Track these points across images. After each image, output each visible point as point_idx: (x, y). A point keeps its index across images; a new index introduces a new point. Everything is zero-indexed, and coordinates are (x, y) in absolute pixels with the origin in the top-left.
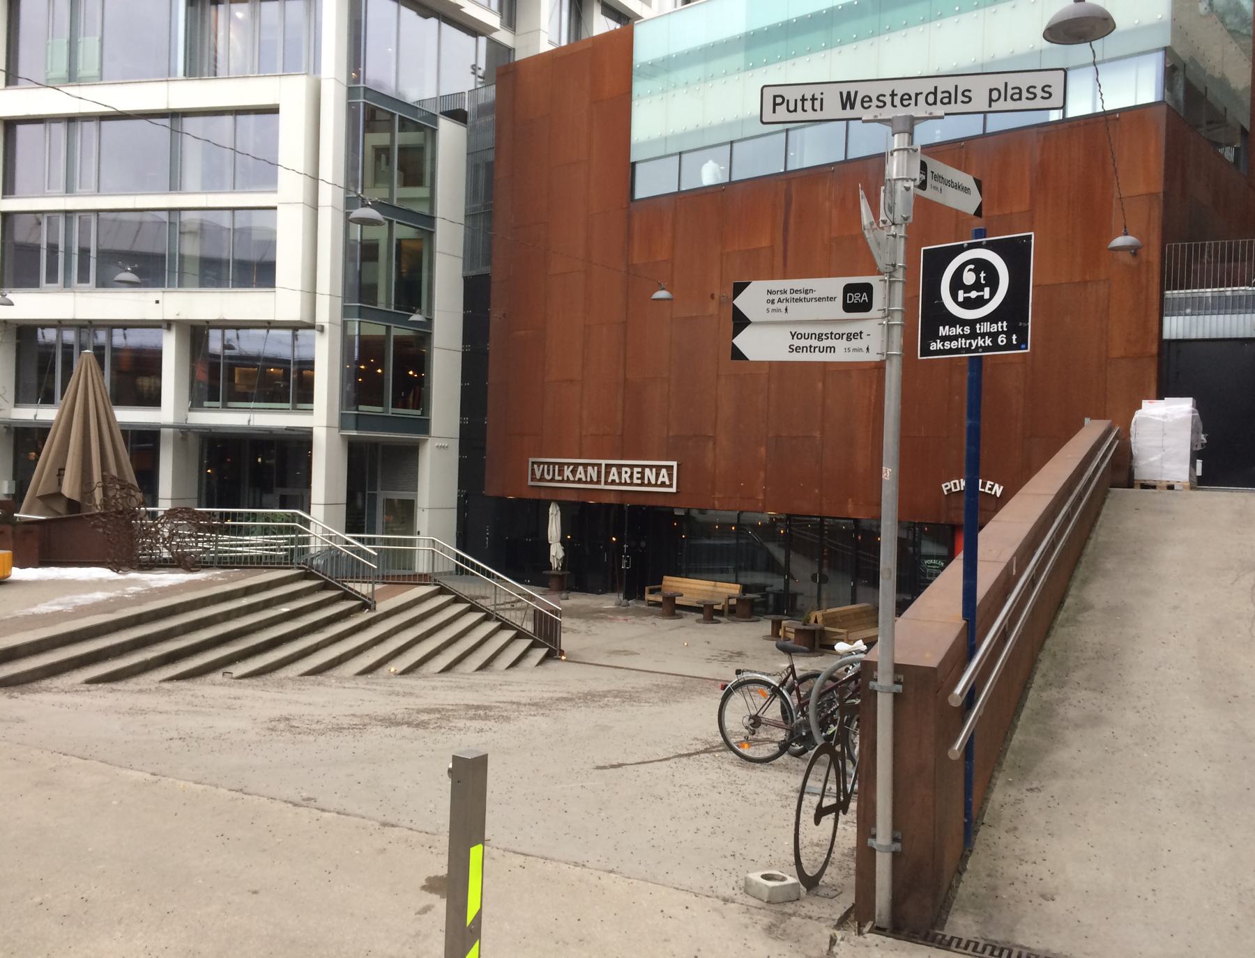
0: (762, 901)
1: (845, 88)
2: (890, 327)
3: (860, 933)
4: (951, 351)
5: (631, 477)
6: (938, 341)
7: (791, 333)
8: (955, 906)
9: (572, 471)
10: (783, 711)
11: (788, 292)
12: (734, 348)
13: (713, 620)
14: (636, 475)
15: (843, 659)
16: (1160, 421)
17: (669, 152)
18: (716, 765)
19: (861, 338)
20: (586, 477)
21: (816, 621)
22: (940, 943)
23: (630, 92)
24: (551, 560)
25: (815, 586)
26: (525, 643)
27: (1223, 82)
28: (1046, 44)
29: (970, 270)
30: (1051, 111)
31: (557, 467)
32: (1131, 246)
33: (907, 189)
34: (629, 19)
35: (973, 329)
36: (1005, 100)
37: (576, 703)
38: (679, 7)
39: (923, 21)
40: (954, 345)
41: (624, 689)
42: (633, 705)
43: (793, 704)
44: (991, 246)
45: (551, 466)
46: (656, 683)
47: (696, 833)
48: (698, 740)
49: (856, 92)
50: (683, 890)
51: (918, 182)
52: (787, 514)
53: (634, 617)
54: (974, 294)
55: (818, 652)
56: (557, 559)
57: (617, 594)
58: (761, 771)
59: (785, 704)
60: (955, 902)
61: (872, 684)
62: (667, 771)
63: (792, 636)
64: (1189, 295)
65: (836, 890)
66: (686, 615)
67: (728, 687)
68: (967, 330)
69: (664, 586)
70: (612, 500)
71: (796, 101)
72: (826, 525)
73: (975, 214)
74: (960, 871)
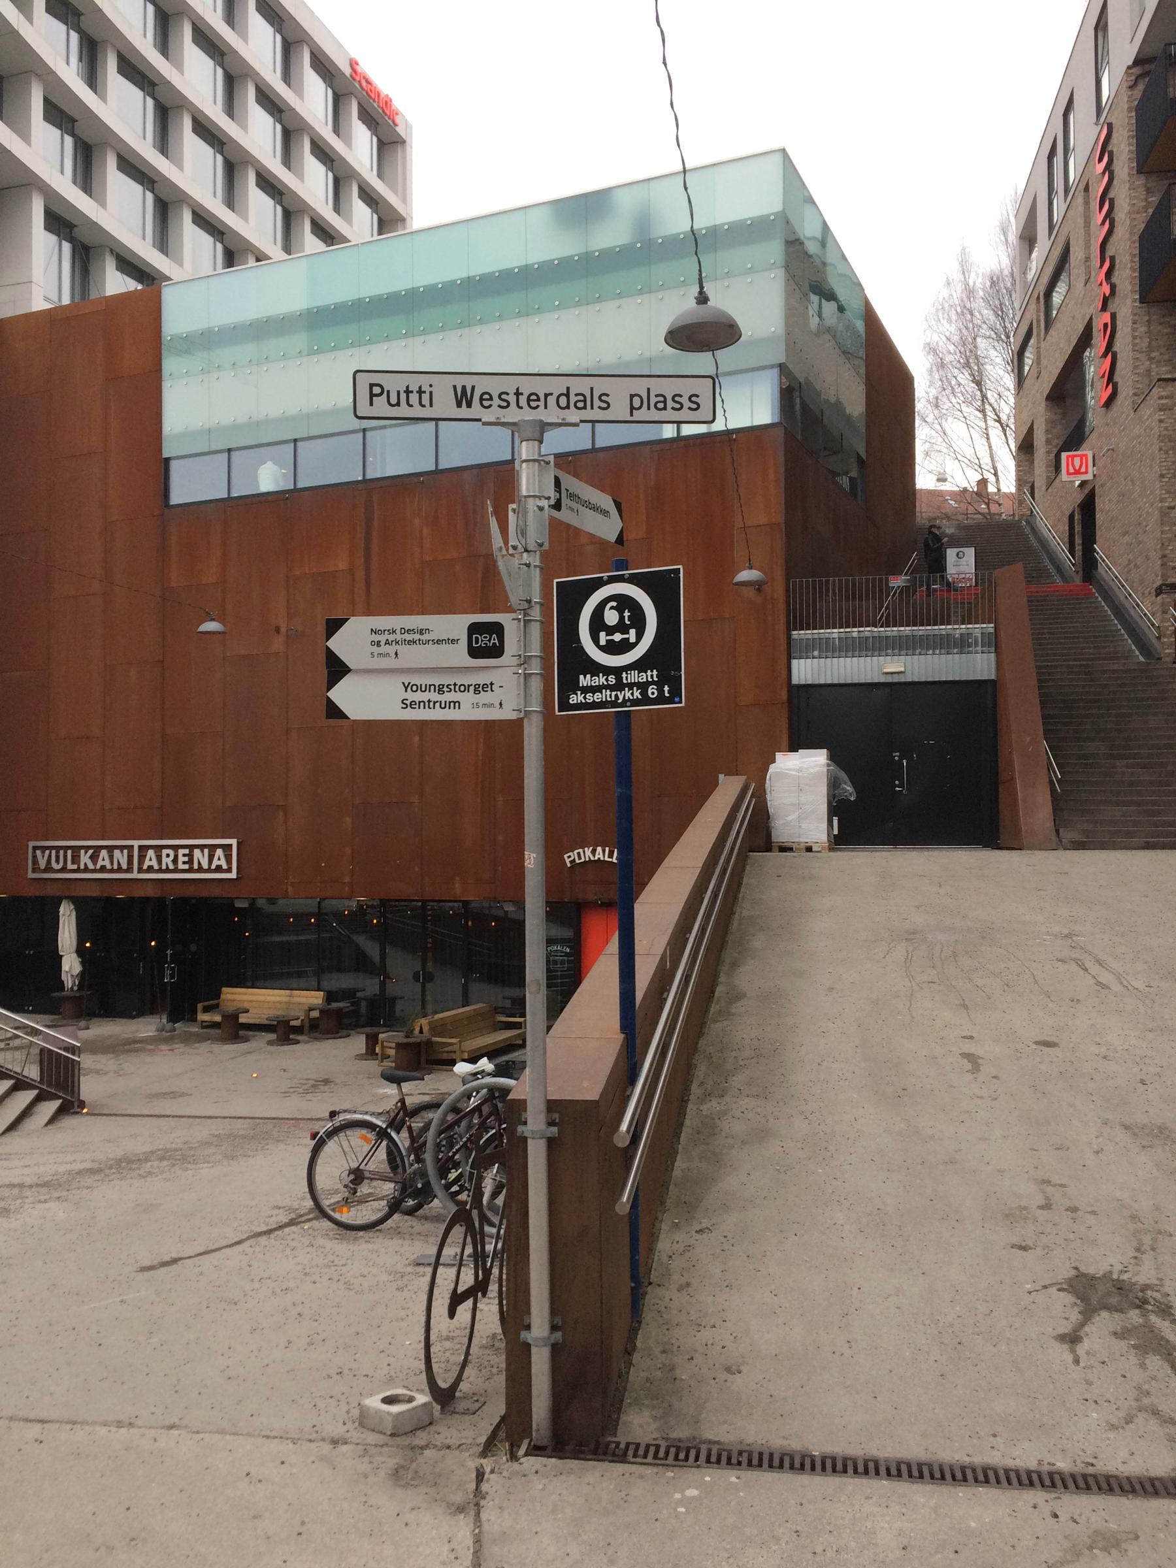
0: (385, 1434)
1: (460, 381)
2: (527, 676)
3: (513, 1457)
4: (594, 705)
5: (175, 861)
6: (579, 693)
7: (403, 683)
8: (627, 1401)
9: (91, 857)
10: (390, 1153)
11: (398, 632)
12: (330, 703)
13: (290, 1040)
14: (181, 859)
15: (467, 1086)
16: (795, 775)
17: (214, 448)
18: (306, 1241)
19: (492, 691)
20: (112, 864)
21: (421, 1031)
22: (614, 1454)
23: (158, 370)
24: (64, 977)
25: (418, 986)
26: (28, 1096)
27: (838, 406)
28: (670, 350)
29: (612, 608)
30: (665, 425)
31: (69, 852)
32: (757, 581)
33: (541, 509)
34: (153, 279)
35: (619, 679)
36: (649, 409)
37: (106, 1175)
38: (220, 270)
39: (519, 315)
40: (597, 697)
41: (173, 1146)
42: (187, 1169)
43: (404, 1146)
44: (634, 580)
45: (62, 852)
46: (217, 1133)
47: (287, 1347)
48: (280, 1208)
49: (473, 387)
50: (276, 1437)
51: (552, 502)
52: (381, 900)
53: (182, 1045)
54: (617, 637)
55: (425, 1068)
56: (72, 976)
57: (159, 1016)
58: (366, 1242)
59: (393, 1148)
60: (627, 1395)
61: (520, 1129)
62: (241, 1261)
63: (392, 1052)
64: (816, 636)
65: (477, 1401)
66: (254, 1036)
67: (319, 1135)
68: (612, 680)
69: (224, 1000)
70: (151, 892)
71: (398, 393)
72: (429, 910)
73: (616, 542)
74: (629, 1351)
